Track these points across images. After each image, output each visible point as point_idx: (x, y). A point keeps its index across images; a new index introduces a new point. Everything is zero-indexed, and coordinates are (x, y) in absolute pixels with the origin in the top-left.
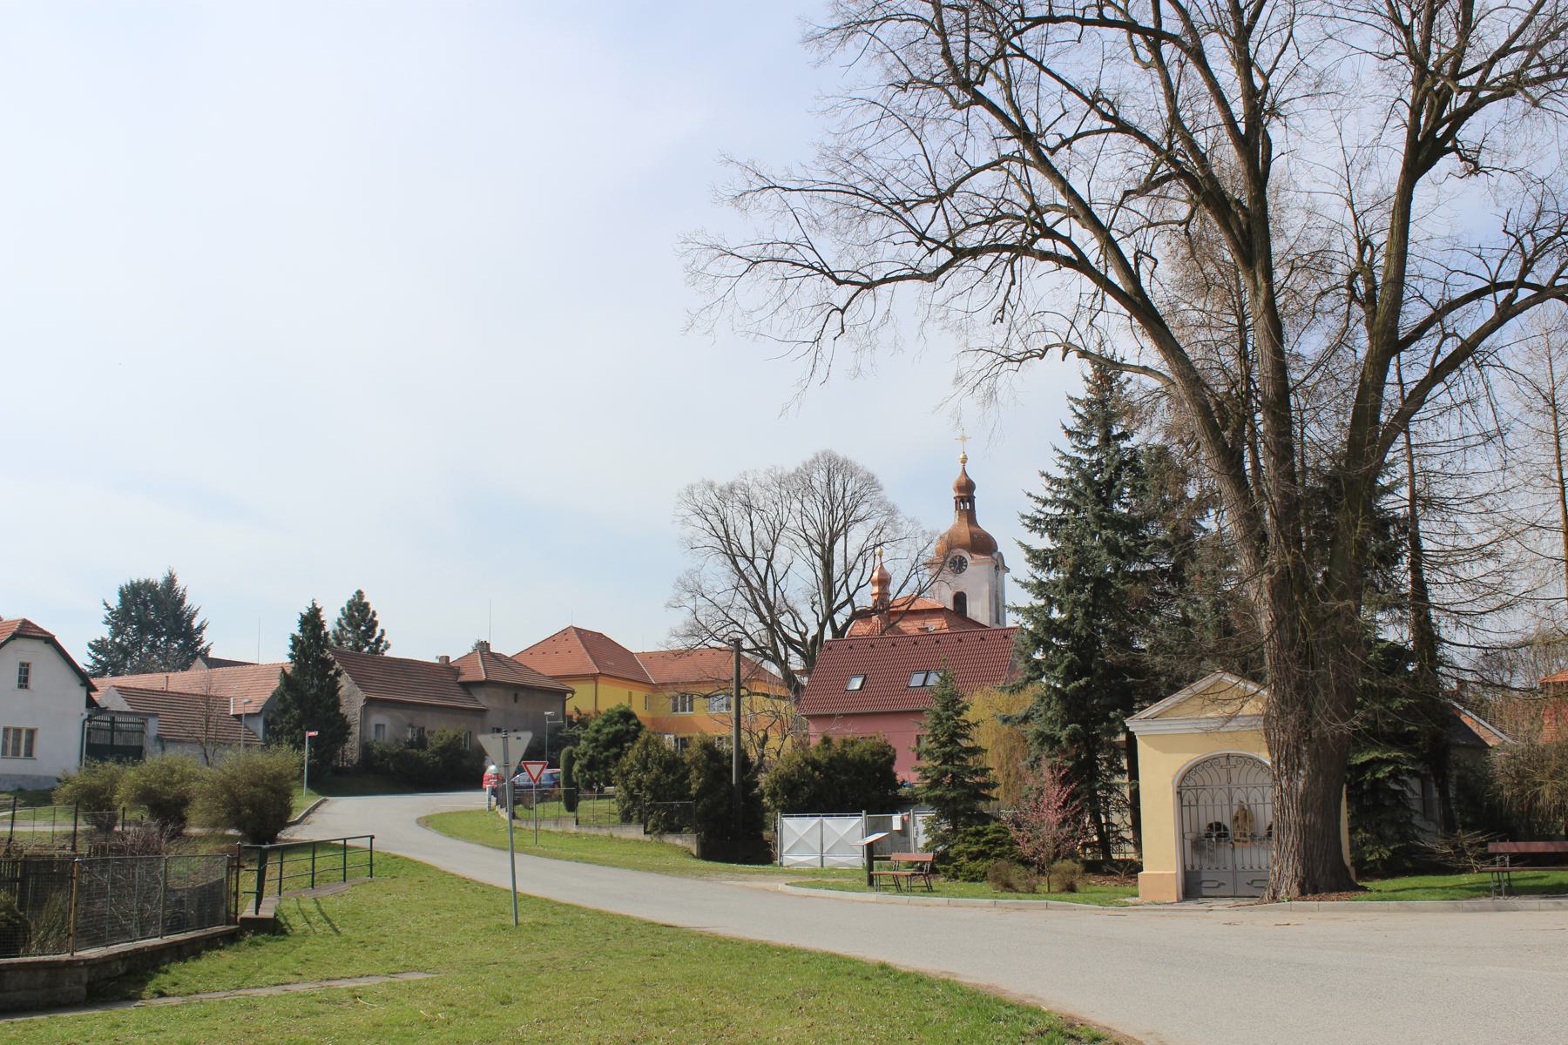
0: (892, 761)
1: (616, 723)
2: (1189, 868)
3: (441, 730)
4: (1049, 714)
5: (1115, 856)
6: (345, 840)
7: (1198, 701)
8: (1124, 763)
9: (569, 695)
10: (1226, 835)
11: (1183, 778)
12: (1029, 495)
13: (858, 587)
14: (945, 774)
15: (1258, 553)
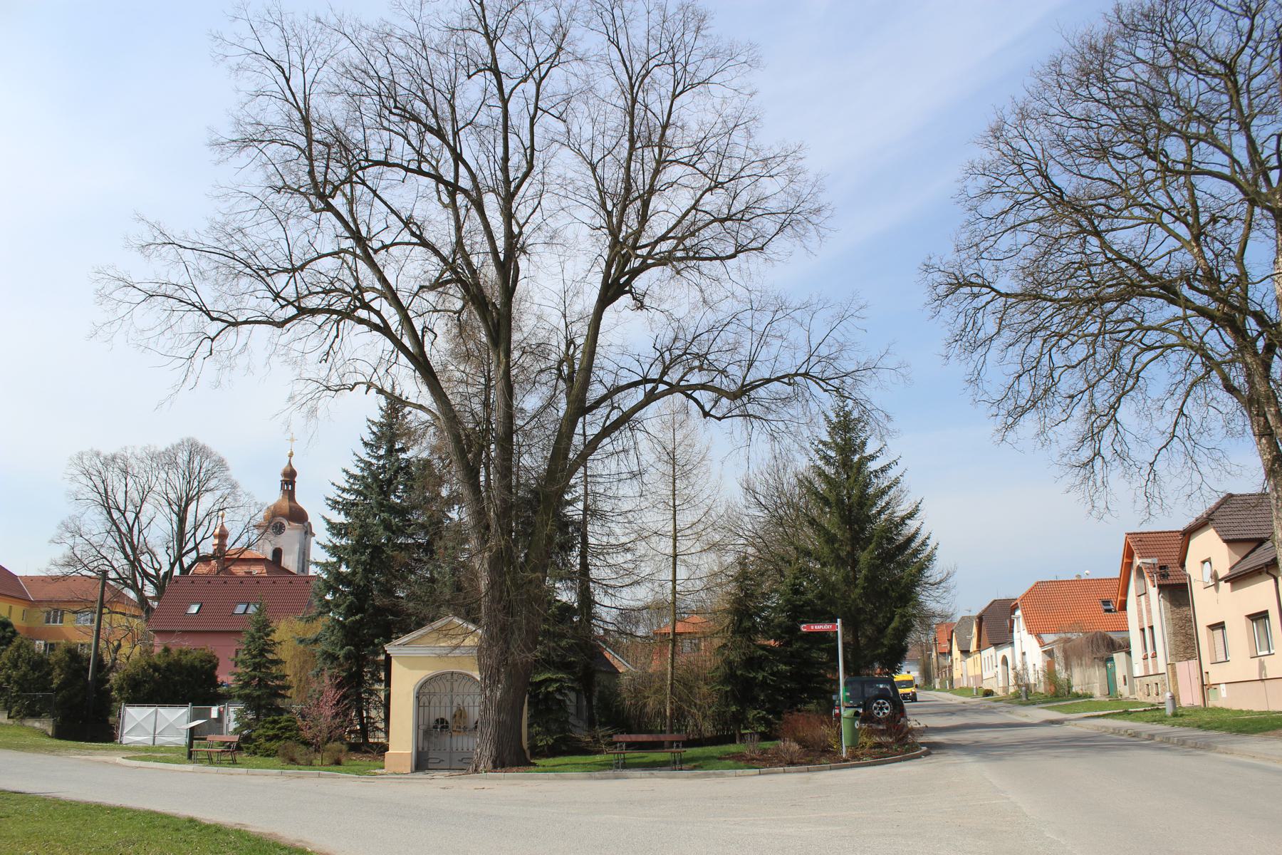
0: (215, 667)
4: (333, 638)
5: (371, 740)
7: (435, 635)
8: (383, 675)
10: (447, 727)
11: (421, 687)
12: (333, 484)
13: (203, 539)
14: (254, 678)
15: (483, 538)
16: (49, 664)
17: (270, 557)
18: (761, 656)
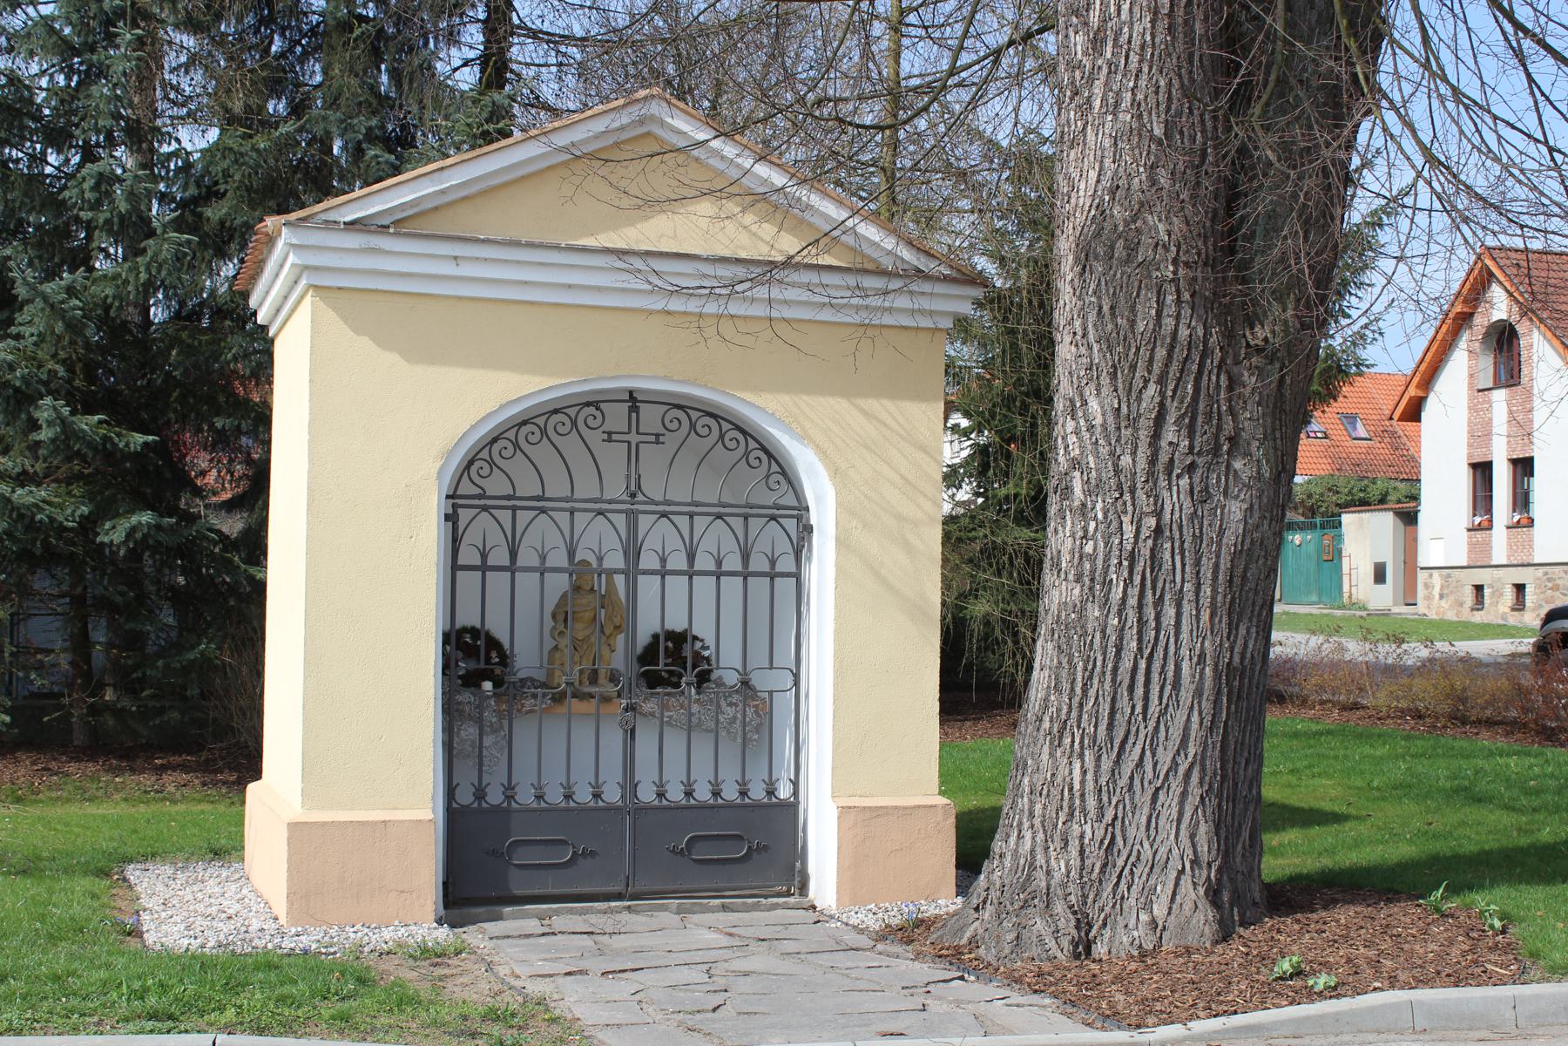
2: (465, 797)
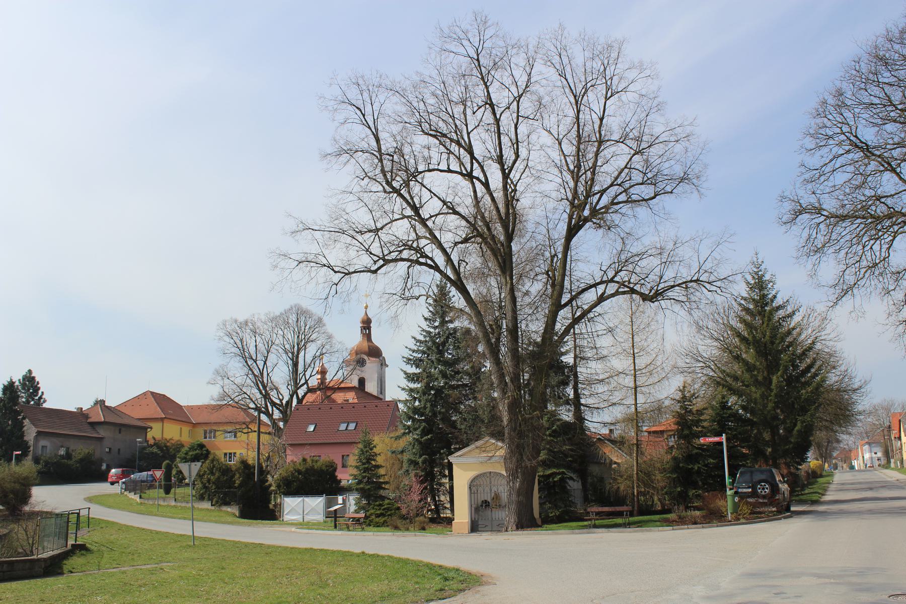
0: (335, 470)
1: (196, 450)
2: (473, 519)
3: (80, 450)
4: (414, 450)
5: (442, 515)
6: (79, 510)
7: (477, 451)
8: (447, 472)
9: (149, 430)
10: (489, 505)
11: (472, 482)
12: (406, 347)
13: (311, 376)
14: (364, 477)
15: (503, 391)
16: (232, 470)
17: (357, 386)
18: (696, 453)
